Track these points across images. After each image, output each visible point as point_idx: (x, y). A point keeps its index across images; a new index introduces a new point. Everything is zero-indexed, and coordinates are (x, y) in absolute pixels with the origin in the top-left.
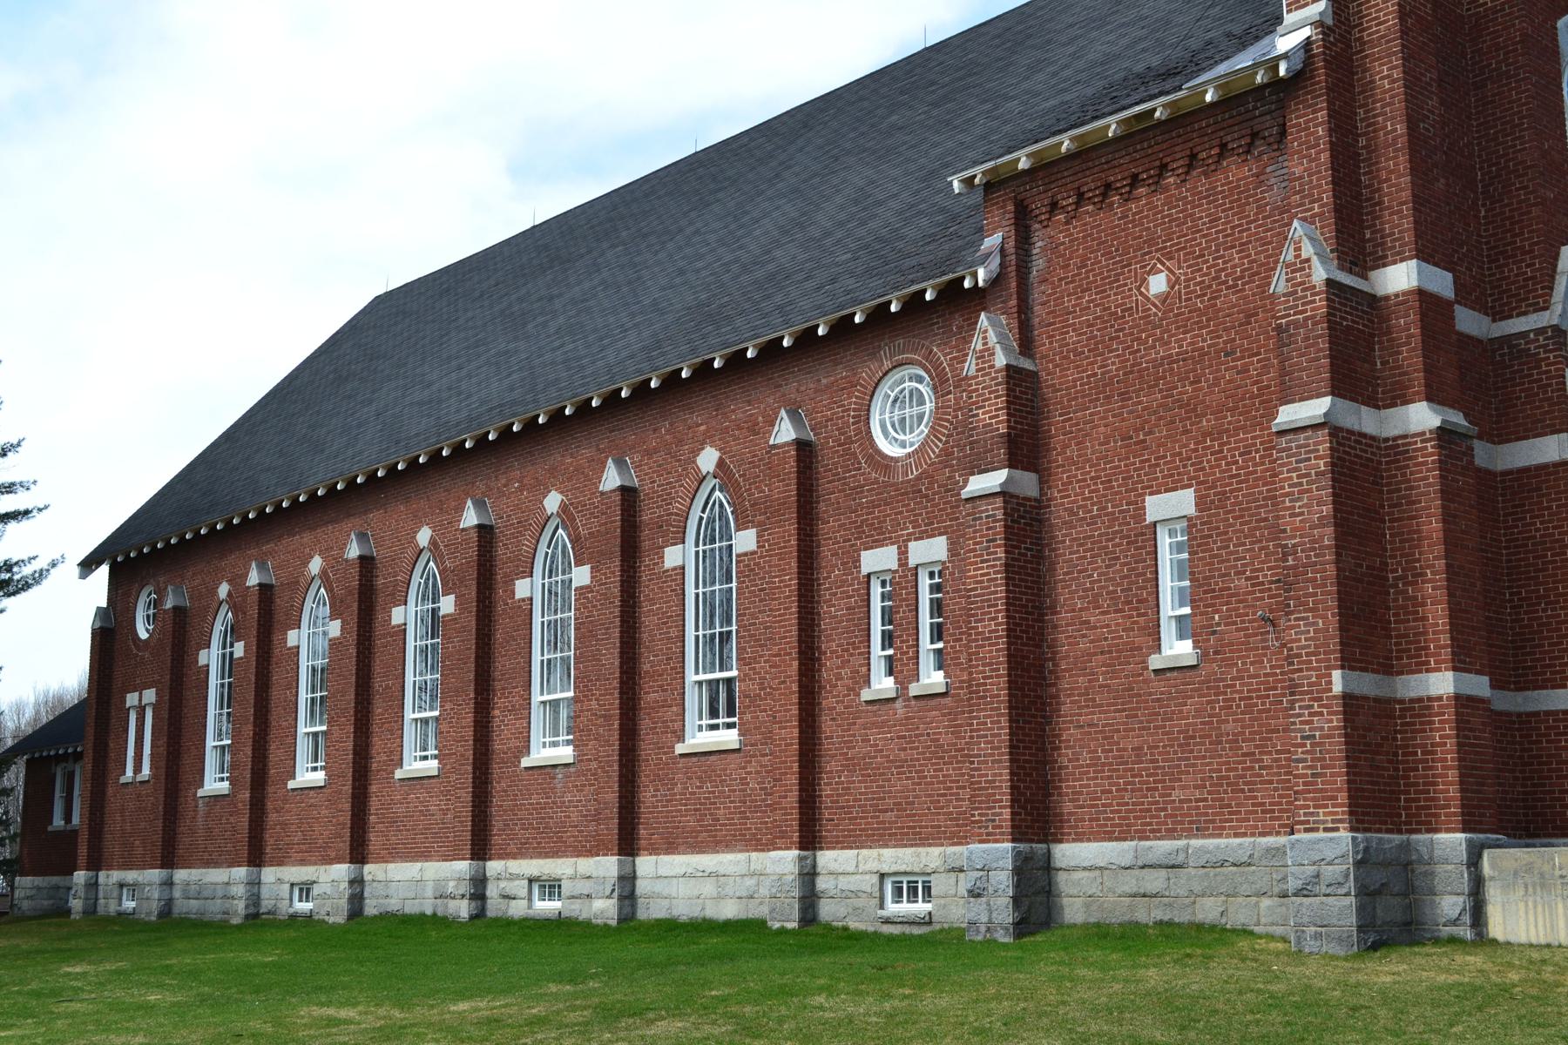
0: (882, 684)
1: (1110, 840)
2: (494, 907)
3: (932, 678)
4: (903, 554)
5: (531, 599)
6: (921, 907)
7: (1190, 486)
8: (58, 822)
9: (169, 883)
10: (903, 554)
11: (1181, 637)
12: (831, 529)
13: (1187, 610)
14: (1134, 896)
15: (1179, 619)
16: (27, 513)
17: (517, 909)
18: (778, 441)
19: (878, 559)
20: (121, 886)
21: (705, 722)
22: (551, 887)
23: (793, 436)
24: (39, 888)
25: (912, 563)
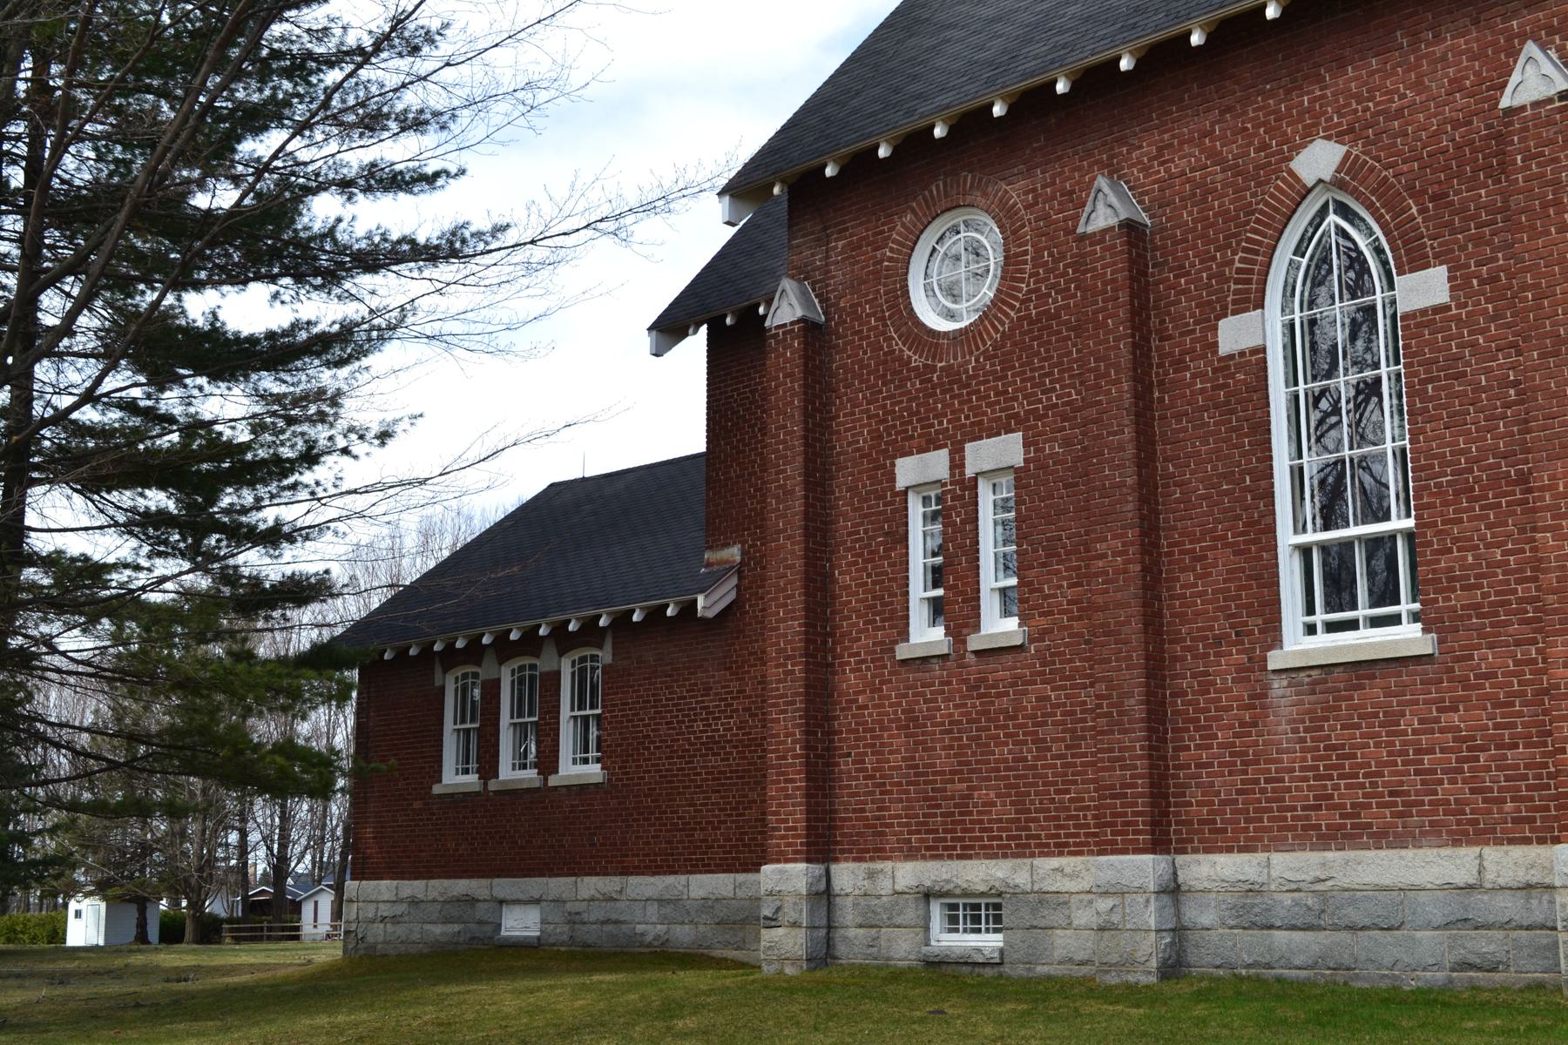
0: (926, 635)
1: (1113, 852)
2: (853, 940)
3: (999, 625)
4: (957, 464)
5: (1263, 350)
6: (989, 942)
7: (945, 446)
8: (455, 777)
9: (824, 896)
10: (957, 464)
11: (1006, 613)
12: (853, 430)
13: (1013, 581)
14: (603, 923)
15: (1003, 591)
16: (431, 180)
17: (902, 948)
18: (1090, 229)
19: (917, 469)
20: (928, 895)
21: (1320, 617)
22: (977, 910)
23: (799, 313)
24: (414, 902)
25: (969, 472)
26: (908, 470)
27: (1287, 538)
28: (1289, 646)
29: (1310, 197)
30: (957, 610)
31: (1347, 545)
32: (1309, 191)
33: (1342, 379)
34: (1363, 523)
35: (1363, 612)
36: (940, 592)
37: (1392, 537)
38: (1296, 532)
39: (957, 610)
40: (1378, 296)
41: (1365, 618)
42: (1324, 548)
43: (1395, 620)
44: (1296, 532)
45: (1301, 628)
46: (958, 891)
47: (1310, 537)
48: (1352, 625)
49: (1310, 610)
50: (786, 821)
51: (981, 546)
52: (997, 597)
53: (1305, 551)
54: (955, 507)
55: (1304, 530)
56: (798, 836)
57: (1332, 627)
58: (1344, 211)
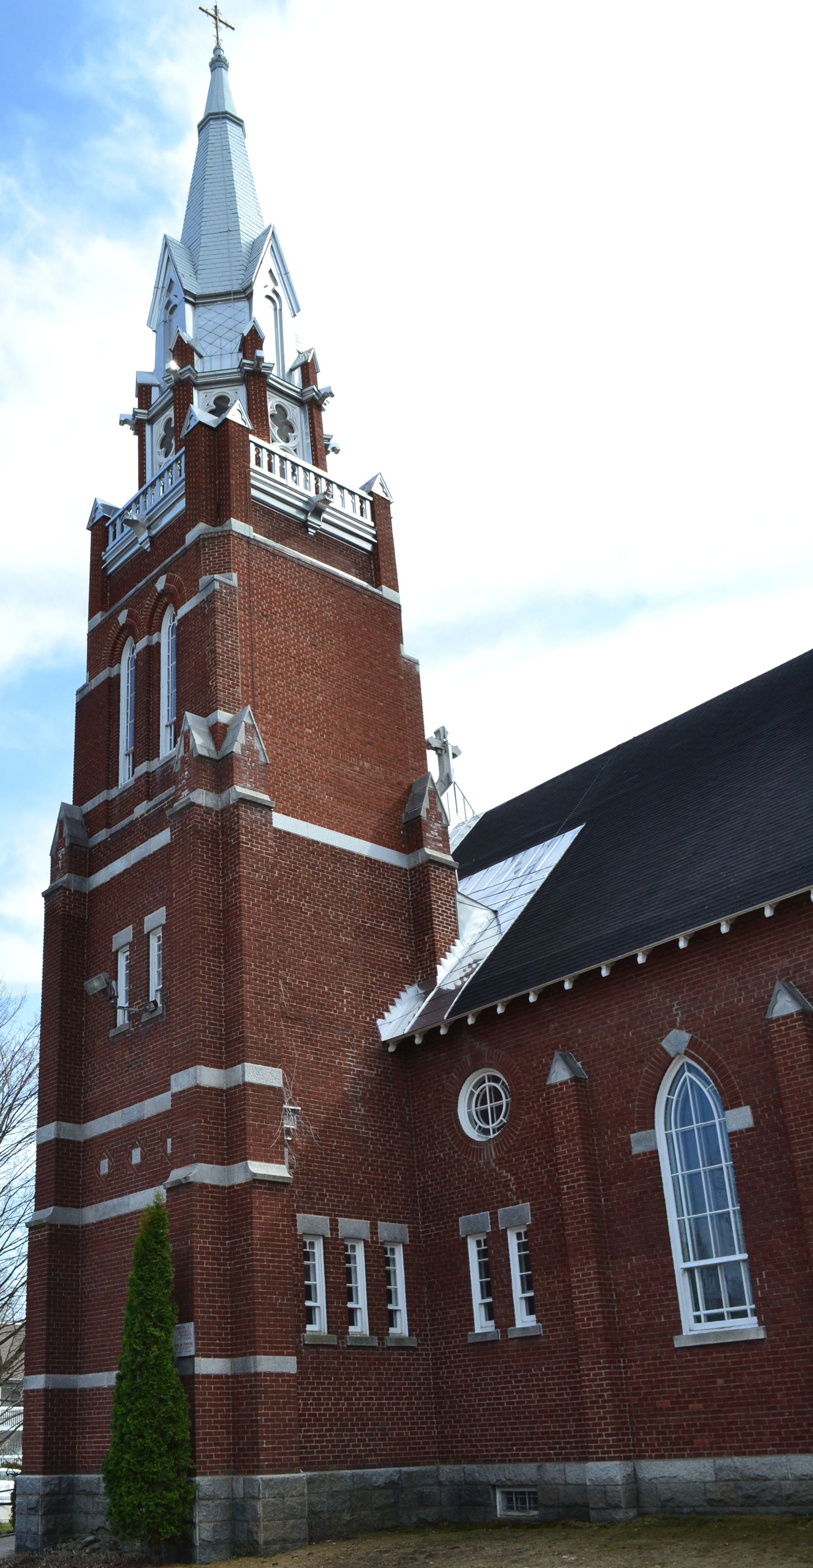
0: (482, 1324)
3: (524, 1320)
21: (703, 1312)
26: (464, 1222)
27: (679, 1264)
28: (686, 1331)
29: (674, 1062)
30: (501, 1310)
31: (714, 1267)
32: (673, 1059)
33: (695, 1125)
34: (723, 1255)
35: (726, 1309)
36: (490, 1300)
37: (737, 1262)
38: (684, 1261)
39: (501, 1310)
40: (717, 1120)
41: (728, 1312)
42: (702, 1269)
43: (743, 1314)
44: (684, 1261)
45: (692, 1319)
46: (509, 1483)
47: (692, 1264)
48: (720, 1317)
49: (697, 1308)
50: (602, 1447)
51: (512, 1273)
52: (524, 1302)
53: (690, 1271)
54: (140, 944)
55: (689, 1260)
56: (202, 1451)
57: (710, 1318)
58: (691, 1069)
